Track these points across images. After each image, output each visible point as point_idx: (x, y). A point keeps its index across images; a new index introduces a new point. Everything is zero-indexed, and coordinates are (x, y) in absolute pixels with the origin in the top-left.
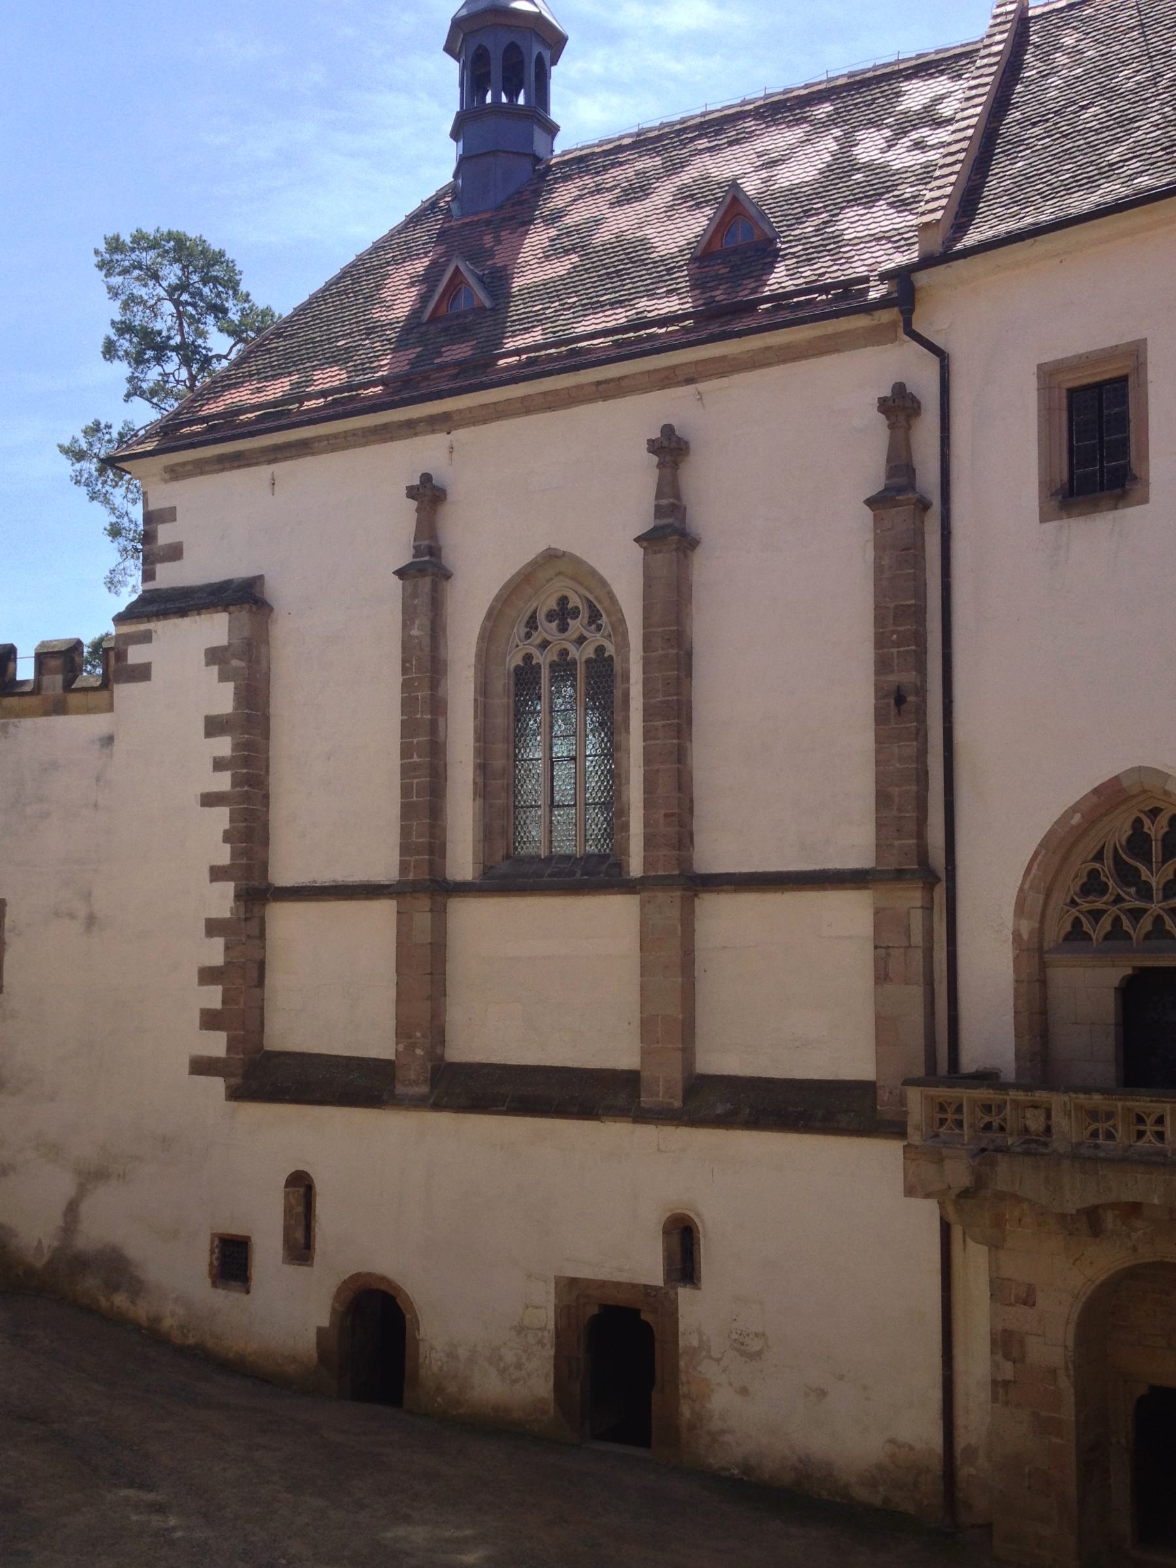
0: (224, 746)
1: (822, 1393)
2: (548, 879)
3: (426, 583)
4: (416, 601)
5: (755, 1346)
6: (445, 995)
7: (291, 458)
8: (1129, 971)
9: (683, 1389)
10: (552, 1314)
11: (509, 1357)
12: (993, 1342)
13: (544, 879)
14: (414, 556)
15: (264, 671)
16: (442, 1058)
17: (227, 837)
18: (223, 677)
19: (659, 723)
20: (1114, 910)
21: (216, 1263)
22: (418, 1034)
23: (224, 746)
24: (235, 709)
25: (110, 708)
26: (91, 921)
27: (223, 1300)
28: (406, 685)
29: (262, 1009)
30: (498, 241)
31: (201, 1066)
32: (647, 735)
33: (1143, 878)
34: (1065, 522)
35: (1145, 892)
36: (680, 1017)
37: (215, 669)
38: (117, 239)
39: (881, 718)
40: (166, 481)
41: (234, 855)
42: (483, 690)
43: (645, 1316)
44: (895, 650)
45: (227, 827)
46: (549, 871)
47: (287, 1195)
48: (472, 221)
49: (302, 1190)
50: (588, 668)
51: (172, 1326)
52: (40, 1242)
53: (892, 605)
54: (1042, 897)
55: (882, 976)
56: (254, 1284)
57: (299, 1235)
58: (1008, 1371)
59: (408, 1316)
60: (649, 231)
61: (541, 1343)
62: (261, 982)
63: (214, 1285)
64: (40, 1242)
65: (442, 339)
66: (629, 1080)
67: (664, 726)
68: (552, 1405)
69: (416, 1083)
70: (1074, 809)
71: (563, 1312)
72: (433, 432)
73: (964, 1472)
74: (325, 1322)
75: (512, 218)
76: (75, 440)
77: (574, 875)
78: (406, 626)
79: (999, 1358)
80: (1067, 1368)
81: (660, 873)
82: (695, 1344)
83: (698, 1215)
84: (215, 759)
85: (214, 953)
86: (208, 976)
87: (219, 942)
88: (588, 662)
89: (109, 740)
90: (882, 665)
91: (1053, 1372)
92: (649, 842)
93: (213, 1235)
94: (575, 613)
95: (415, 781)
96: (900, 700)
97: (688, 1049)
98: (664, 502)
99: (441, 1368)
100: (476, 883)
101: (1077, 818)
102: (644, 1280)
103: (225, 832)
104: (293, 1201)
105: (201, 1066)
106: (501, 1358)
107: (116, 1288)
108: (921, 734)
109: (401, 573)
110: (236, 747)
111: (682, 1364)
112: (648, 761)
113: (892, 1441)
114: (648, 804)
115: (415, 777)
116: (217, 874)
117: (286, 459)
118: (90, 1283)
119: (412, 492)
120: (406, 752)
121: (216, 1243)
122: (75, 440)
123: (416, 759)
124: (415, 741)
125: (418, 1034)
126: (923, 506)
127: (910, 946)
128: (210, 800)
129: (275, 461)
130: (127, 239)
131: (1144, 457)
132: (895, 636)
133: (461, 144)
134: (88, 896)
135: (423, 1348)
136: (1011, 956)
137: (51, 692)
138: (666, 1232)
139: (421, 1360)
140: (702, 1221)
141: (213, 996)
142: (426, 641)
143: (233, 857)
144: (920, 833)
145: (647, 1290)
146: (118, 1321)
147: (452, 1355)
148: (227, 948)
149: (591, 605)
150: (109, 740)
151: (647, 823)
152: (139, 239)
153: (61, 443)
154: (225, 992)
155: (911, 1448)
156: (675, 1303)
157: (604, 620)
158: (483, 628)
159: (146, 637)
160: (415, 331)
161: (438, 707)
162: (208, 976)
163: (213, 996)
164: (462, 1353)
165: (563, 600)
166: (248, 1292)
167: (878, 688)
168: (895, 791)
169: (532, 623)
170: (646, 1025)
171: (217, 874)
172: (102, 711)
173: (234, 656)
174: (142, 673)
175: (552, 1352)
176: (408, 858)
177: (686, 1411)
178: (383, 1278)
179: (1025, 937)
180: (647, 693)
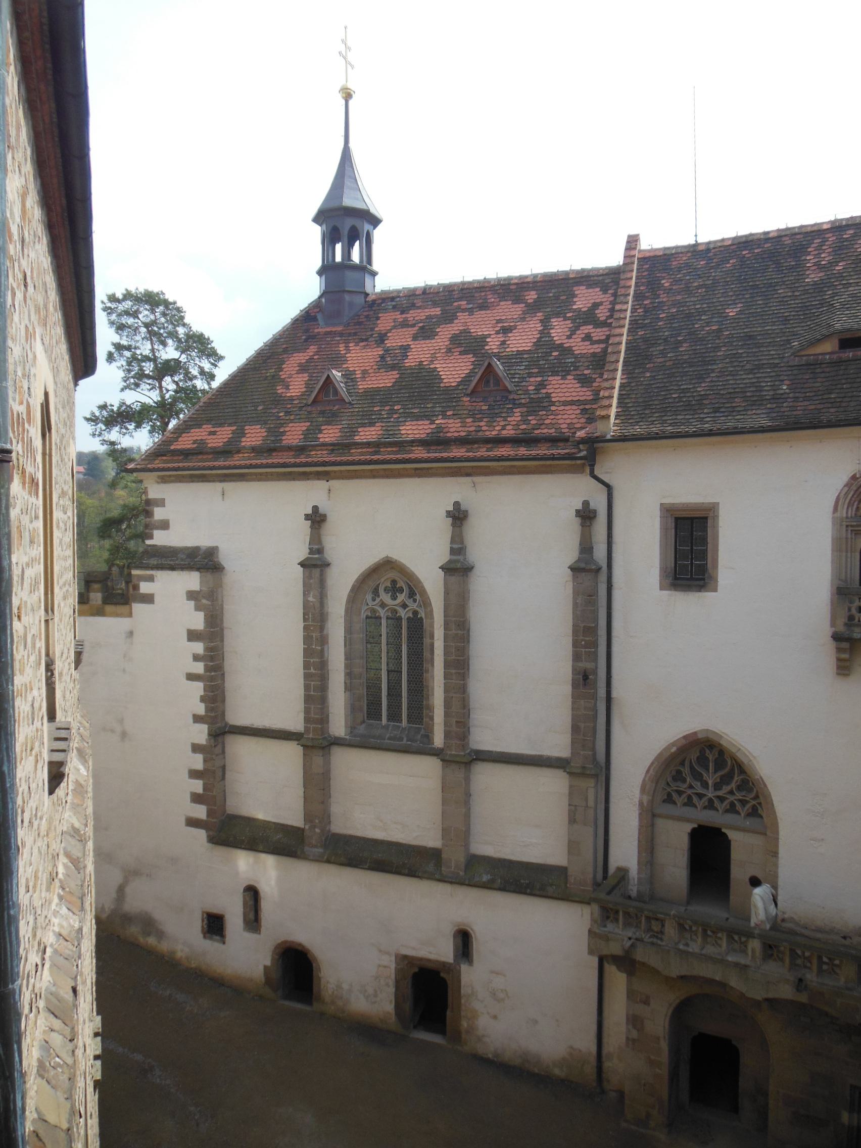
0: (199, 647)
1: (536, 1022)
2: (389, 741)
3: (316, 572)
4: (311, 581)
5: (502, 995)
6: (330, 797)
7: (234, 481)
8: (696, 826)
9: (463, 1014)
10: (393, 971)
11: (370, 991)
12: (628, 1019)
13: (386, 741)
14: (310, 554)
15: (220, 603)
16: (329, 831)
17: (203, 699)
18: (198, 608)
19: (454, 671)
20: (689, 792)
21: (205, 926)
22: (317, 821)
23: (199, 647)
24: (205, 628)
25: (130, 615)
26: (124, 735)
27: (210, 946)
28: (306, 628)
29: (225, 791)
30: (347, 348)
31: (192, 822)
32: (446, 676)
33: (704, 778)
34: (673, 593)
35: (705, 785)
36: (464, 829)
37: (193, 603)
38: (114, 295)
39: (575, 685)
40: (158, 483)
41: (207, 709)
42: (349, 630)
43: (442, 975)
44: (583, 650)
45: (202, 693)
46: (388, 736)
47: (244, 896)
48: (332, 331)
49: (252, 893)
50: (408, 622)
51: (181, 957)
52: (103, 905)
53: (582, 625)
54: (654, 785)
55: (572, 820)
56: (227, 939)
57: (252, 916)
58: (634, 1034)
59: (314, 965)
60: (437, 365)
61: (387, 985)
62: (223, 778)
63: (205, 937)
64: (103, 905)
65: (321, 419)
66: (434, 855)
67: (457, 673)
68: (394, 1015)
69: (316, 846)
70: (673, 744)
71: (398, 971)
72: (319, 479)
73: (607, 1064)
74: (268, 963)
75: (355, 334)
76: (93, 414)
77: (402, 740)
78: (305, 594)
79: (630, 1027)
80: (665, 1037)
81: (453, 753)
82: (470, 992)
83: (472, 929)
84: (194, 654)
85: (198, 762)
86: (194, 774)
87: (199, 758)
88: (409, 618)
89: (131, 634)
90: (576, 657)
91: (658, 1038)
92: (447, 734)
93: (203, 912)
94: (401, 590)
95: (312, 683)
96: (586, 677)
97: (467, 846)
98: (455, 546)
99: (333, 992)
100: (346, 739)
101: (674, 749)
102: (443, 959)
103: (201, 696)
104: (248, 899)
105: (192, 822)
106: (366, 991)
107: (149, 934)
108: (594, 697)
109: (302, 564)
110: (207, 649)
111: (463, 1001)
112: (446, 691)
113: (571, 1047)
114: (447, 715)
115: (313, 681)
116: (197, 719)
117: (231, 481)
118: (134, 930)
119: (307, 517)
120: (306, 666)
121: (205, 916)
122: (93, 414)
123: (312, 670)
124: (312, 660)
125: (317, 821)
126: (599, 570)
127: (587, 806)
128: (191, 677)
129: (224, 481)
130: (119, 295)
131: (715, 566)
132: (583, 643)
133: (324, 277)
134: (121, 721)
135: (323, 981)
136: (637, 812)
137: (94, 603)
138: (455, 936)
139: (322, 987)
140: (475, 934)
141: (198, 786)
142: (317, 605)
143: (206, 711)
144: (593, 749)
145: (444, 964)
146: (150, 952)
147: (339, 987)
148: (205, 761)
149: (410, 587)
150: (131, 634)
151: (446, 724)
152: (128, 296)
153: (85, 416)
154: (204, 785)
155: (580, 1051)
156: (459, 972)
157: (418, 597)
158: (349, 596)
159: (151, 579)
160: (304, 409)
161: (323, 640)
162: (194, 774)
163: (198, 786)
164: (345, 986)
165: (394, 582)
166: (224, 943)
167: (574, 670)
168: (582, 725)
169: (376, 592)
170: (444, 830)
171: (197, 719)
172: (125, 617)
173: (204, 597)
174: (148, 599)
175: (394, 990)
176: (309, 725)
177: (465, 1024)
178: (300, 945)
179: (645, 804)
180: (446, 653)
